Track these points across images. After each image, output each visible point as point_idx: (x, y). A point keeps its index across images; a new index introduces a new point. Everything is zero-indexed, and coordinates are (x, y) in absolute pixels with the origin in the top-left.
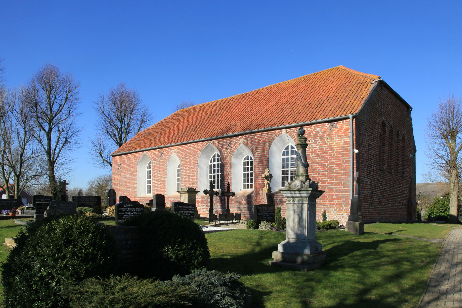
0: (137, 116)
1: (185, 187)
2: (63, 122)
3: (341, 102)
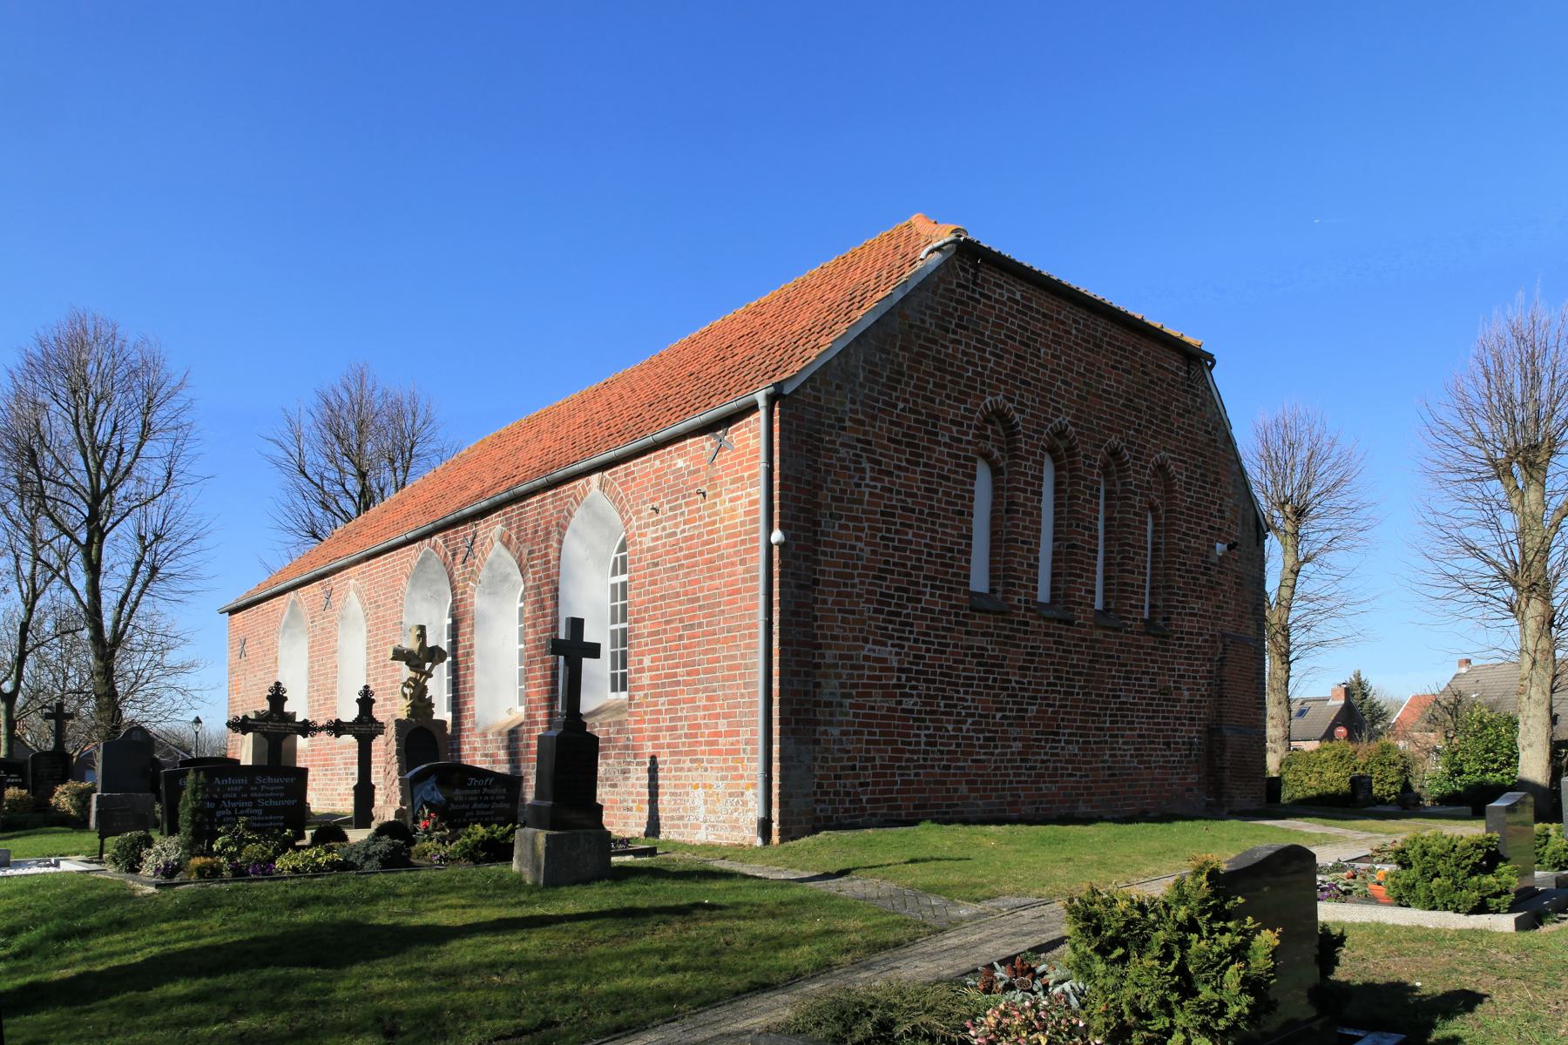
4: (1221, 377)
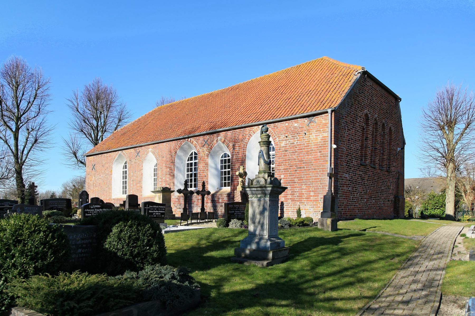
0: (114, 113)
1: (159, 187)
2: (32, 120)
3: (321, 96)
4: (401, 104)
